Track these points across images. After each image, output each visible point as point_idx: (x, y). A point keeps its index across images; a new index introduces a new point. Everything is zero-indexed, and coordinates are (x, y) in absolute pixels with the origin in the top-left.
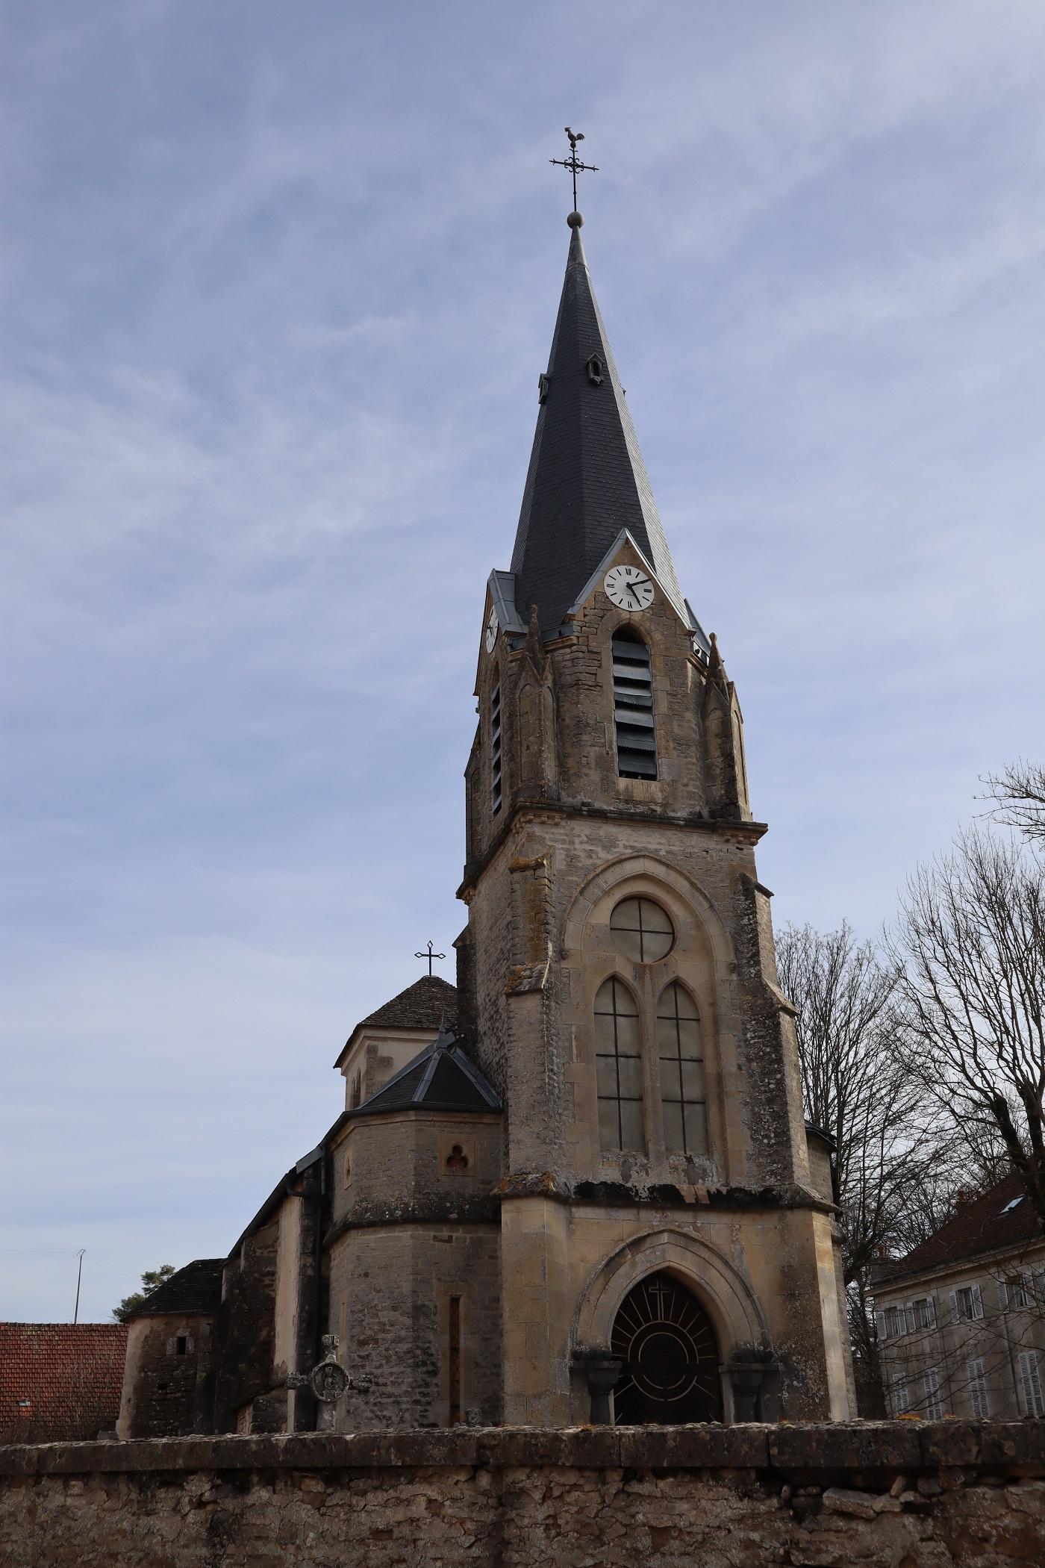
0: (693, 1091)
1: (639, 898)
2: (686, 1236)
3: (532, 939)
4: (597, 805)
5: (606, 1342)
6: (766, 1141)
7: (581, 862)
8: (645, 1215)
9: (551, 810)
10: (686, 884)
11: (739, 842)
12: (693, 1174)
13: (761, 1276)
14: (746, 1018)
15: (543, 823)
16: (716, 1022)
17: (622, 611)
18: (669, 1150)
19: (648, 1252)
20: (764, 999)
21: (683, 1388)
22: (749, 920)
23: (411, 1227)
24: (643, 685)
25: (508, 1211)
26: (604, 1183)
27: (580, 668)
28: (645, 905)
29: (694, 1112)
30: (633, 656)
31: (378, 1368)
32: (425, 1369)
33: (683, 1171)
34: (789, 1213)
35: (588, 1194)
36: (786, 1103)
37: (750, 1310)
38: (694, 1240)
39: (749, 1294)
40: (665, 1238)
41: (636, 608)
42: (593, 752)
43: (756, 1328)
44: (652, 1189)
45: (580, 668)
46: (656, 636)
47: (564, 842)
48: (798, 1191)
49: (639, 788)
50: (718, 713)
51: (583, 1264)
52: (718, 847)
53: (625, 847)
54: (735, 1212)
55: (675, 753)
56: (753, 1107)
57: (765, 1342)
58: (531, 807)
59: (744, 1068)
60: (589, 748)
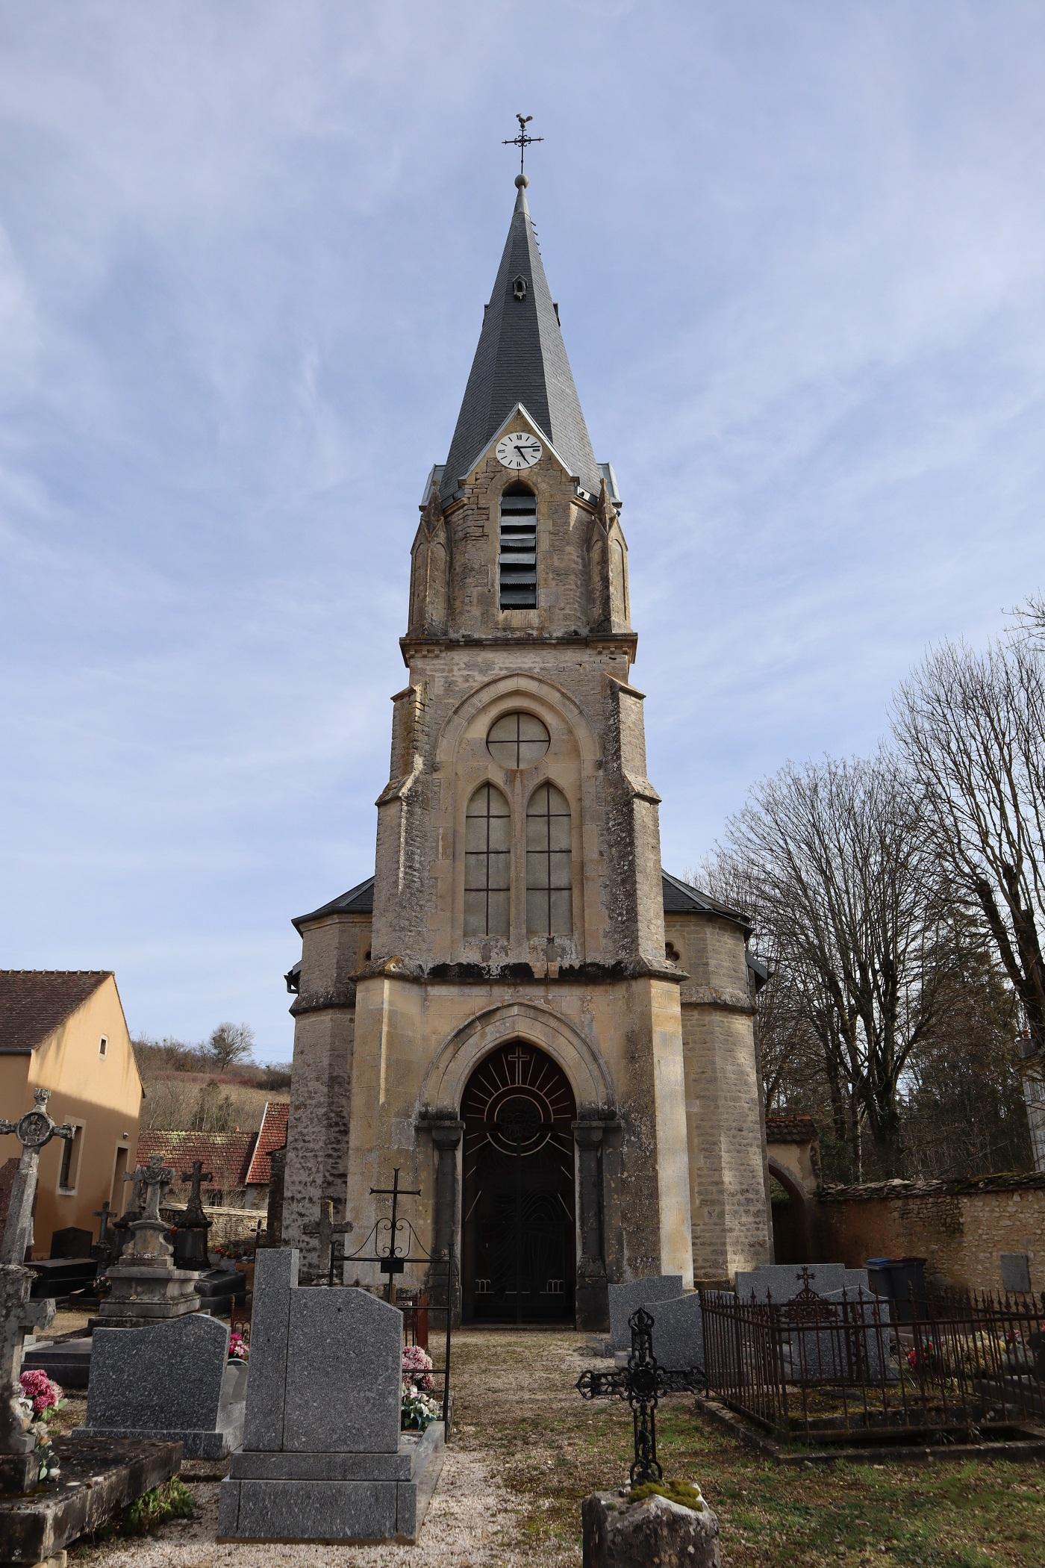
0: (560, 879)
1: (518, 713)
2: (535, 1008)
3: (403, 756)
4: (476, 636)
5: (453, 1104)
6: (620, 919)
7: (457, 686)
8: (497, 991)
9: (428, 644)
10: (558, 695)
11: (612, 653)
12: (551, 949)
13: (610, 1042)
14: (609, 808)
15: (425, 657)
16: (581, 816)
17: (510, 471)
18: (531, 932)
19: (498, 1024)
20: (623, 789)
21: (536, 1144)
22: (614, 719)
23: (330, 1011)
24: (531, 529)
25: (361, 992)
26: (460, 965)
27: (469, 523)
28: (522, 719)
29: (560, 899)
30: (520, 507)
31: (305, 1128)
32: (337, 1129)
33: (542, 950)
34: (633, 983)
35: (441, 974)
36: (636, 882)
37: (596, 1073)
38: (543, 1011)
39: (595, 1059)
40: (515, 1010)
41: (524, 465)
42: (475, 592)
43: (602, 1088)
44: (504, 968)
45: (469, 523)
46: (542, 487)
47: (443, 671)
48: (640, 962)
49: (517, 617)
50: (600, 544)
51: (434, 1036)
52: (592, 659)
53: (501, 669)
54: (587, 985)
55: (554, 583)
56: (611, 889)
57: (610, 1102)
58: (410, 644)
59: (605, 854)
60: (472, 589)
